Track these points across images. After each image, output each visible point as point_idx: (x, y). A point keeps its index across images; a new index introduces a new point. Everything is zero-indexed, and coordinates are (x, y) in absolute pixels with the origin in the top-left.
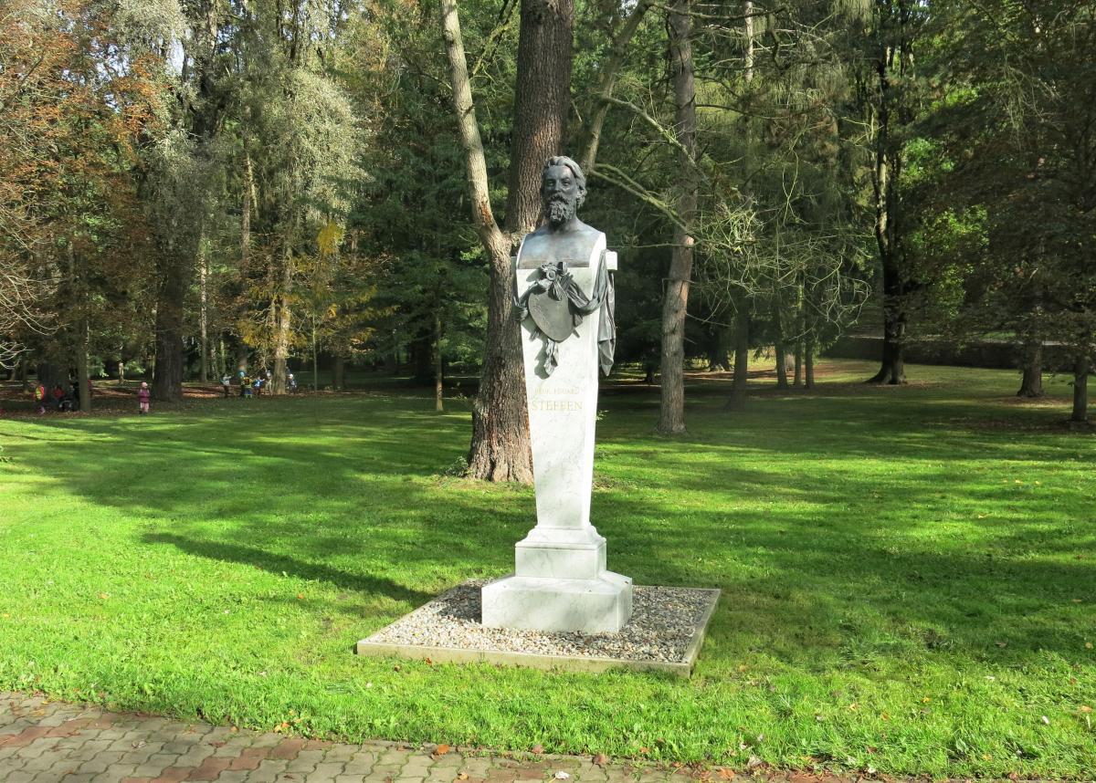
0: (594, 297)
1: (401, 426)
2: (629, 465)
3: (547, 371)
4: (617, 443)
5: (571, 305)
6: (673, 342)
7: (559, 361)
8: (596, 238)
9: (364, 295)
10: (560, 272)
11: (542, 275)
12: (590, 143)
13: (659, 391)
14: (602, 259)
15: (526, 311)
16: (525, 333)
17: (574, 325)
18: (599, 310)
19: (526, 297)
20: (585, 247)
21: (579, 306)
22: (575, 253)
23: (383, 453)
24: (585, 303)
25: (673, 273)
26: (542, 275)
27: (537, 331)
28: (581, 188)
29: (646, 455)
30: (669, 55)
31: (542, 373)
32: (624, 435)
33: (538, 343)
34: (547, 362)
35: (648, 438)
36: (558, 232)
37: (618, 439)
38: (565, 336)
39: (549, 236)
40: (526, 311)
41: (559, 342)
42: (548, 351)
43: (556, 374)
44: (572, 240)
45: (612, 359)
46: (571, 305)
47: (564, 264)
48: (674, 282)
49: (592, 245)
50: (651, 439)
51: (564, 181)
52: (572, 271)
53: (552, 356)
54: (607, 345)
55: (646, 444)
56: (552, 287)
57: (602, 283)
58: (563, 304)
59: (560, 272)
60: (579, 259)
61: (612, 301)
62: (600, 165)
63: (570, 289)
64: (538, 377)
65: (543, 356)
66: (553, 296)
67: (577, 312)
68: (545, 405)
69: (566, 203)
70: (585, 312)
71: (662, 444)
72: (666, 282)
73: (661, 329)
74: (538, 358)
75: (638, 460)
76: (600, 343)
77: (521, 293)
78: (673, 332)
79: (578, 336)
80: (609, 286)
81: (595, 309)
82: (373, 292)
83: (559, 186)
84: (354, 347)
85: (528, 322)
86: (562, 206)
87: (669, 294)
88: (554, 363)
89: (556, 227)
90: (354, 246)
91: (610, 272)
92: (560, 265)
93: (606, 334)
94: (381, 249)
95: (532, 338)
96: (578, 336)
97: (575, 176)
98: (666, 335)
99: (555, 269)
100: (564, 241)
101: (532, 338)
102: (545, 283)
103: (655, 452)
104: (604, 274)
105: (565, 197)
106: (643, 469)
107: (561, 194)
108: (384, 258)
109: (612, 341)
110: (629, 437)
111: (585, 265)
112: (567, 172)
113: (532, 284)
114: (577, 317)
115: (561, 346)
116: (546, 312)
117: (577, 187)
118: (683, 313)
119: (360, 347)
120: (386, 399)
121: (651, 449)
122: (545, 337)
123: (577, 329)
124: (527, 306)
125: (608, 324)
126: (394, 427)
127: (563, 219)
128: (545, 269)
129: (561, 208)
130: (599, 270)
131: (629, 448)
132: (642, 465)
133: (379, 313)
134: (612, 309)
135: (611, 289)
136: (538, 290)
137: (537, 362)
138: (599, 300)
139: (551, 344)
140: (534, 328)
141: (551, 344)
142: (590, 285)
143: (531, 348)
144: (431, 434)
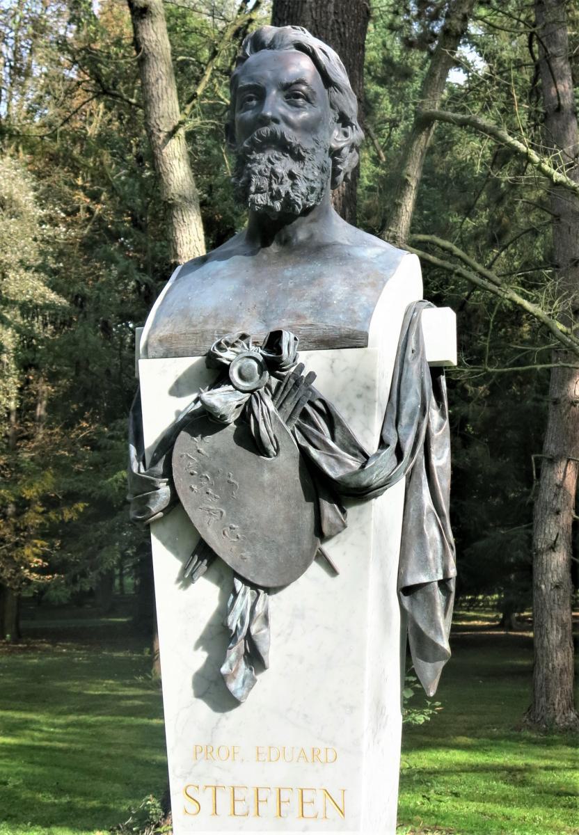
0: (383, 444)
1: (84, 710)
2: (483, 798)
3: (234, 686)
4: (458, 747)
5: (309, 468)
6: (554, 564)
7: (272, 653)
8: (392, 265)
9: (31, 485)
10: (272, 364)
11: (217, 373)
12: (401, 195)
13: (529, 644)
14: (410, 328)
15: (164, 490)
16: (165, 563)
17: (320, 534)
18: (399, 487)
19: (167, 444)
20: (355, 288)
21: (335, 472)
22: (322, 304)
23: (28, 769)
24: (355, 464)
25: (550, 447)
26: (217, 373)
27: (202, 554)
28: (344, 120)
29: (513, 774)
30: (534, 93)
31: (215, 691)
32: (471, 731)
33: (206, 592)
34: (234, 649)
35: (512, 737)
36: (274, 248)
37: (463, 740)
38: (290, 572)
39: (249, 260)
40: (164, 490)
41: (269, 590)
42: (233, 621)
43: (262, 695)
44: (314, 268)
45: (445, 644)
46: (309, 468)
47: (287, 337)
48: (553, 461)
49: (378, 283)
50: (518, 739)
51: (291, 92)
52: (313, 361)
53: (249, 637)
54: (431, 600)
55: (509, 749)
56: (246, 414)
57: (411, 401)
58: (285, 464)
59: (272, 364)
60: (334, 322)
61: (442, 459)
62: (422, 237)
63: (305, 415)
64: (203, 707)
65: (219, 636)
66: (250, 440)
67: (334, 494)
68: (224, 799)
69: (298, 158)
70: (353, 494)
71: (538, 751)
72: (538, 461)
73: (530, 541)
74: (204, 642)
75: (500, 787)
76: (407, 591)
77: (151, 436)
78: (553, 547)
79: (332, 571)
80: (435, 416)
81: (387, 483)
82: (47, 483)
83: (275, 105)
84: (32, 570)
85: (173, 523)
86: (284, 165)
87: (544, 482)
88: (255, 658)
89: (268, 231)
90: (40, 411)
91: (436, 370)
92: (274, 341)
93: (424, 564)
94: (79, 415)
95: (186, 579)
96: (332, 571)
97: (328, 81)
98: (540, 553)
99: (259, 353)
100: (292, 273)
101: (186, 579)
102: (224, 400)
103: (528, 769)
104: (417, 377)
105: (292, 136)
106: (507, 811)
107: (281, 128)
108: (83, 429)
109: (443, 584)
110: (483, 735)
111: (354, 340)
112: (303, 66)
113: (186, 403)
114: (329, 510)
115: (275, 604)
116: (228, 492)
117: (332, 115)
118: (567, 518)
119: (41, 571)
120: (81, 657)
121: (520, 761)
122: (226, 576)
123: (329, 548)
124: (168, 473)
125: (432, 532)
126: (70, 712)
127: (288, 202)
128: (227, 356)
129: (280, 170)
130: (402, 361)
131: (479, 759)
132: (506, 800)
133: (52, 515)
134: (444, 484)
135: (437, 422)
136: (203, 421)
137: (201, 657)
138: (399, 453)
139: (245, 598)
140: (190, 544)
141: (245, 598)
142: (370, 402)
143: (183, 609)
144: (130, 727)
